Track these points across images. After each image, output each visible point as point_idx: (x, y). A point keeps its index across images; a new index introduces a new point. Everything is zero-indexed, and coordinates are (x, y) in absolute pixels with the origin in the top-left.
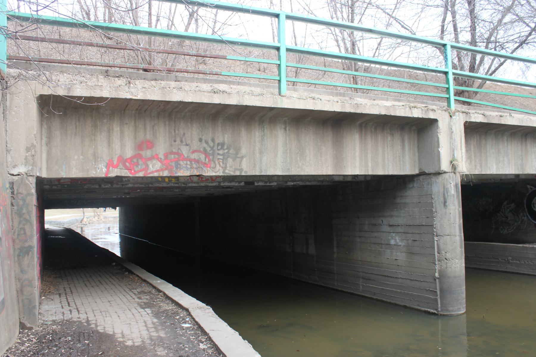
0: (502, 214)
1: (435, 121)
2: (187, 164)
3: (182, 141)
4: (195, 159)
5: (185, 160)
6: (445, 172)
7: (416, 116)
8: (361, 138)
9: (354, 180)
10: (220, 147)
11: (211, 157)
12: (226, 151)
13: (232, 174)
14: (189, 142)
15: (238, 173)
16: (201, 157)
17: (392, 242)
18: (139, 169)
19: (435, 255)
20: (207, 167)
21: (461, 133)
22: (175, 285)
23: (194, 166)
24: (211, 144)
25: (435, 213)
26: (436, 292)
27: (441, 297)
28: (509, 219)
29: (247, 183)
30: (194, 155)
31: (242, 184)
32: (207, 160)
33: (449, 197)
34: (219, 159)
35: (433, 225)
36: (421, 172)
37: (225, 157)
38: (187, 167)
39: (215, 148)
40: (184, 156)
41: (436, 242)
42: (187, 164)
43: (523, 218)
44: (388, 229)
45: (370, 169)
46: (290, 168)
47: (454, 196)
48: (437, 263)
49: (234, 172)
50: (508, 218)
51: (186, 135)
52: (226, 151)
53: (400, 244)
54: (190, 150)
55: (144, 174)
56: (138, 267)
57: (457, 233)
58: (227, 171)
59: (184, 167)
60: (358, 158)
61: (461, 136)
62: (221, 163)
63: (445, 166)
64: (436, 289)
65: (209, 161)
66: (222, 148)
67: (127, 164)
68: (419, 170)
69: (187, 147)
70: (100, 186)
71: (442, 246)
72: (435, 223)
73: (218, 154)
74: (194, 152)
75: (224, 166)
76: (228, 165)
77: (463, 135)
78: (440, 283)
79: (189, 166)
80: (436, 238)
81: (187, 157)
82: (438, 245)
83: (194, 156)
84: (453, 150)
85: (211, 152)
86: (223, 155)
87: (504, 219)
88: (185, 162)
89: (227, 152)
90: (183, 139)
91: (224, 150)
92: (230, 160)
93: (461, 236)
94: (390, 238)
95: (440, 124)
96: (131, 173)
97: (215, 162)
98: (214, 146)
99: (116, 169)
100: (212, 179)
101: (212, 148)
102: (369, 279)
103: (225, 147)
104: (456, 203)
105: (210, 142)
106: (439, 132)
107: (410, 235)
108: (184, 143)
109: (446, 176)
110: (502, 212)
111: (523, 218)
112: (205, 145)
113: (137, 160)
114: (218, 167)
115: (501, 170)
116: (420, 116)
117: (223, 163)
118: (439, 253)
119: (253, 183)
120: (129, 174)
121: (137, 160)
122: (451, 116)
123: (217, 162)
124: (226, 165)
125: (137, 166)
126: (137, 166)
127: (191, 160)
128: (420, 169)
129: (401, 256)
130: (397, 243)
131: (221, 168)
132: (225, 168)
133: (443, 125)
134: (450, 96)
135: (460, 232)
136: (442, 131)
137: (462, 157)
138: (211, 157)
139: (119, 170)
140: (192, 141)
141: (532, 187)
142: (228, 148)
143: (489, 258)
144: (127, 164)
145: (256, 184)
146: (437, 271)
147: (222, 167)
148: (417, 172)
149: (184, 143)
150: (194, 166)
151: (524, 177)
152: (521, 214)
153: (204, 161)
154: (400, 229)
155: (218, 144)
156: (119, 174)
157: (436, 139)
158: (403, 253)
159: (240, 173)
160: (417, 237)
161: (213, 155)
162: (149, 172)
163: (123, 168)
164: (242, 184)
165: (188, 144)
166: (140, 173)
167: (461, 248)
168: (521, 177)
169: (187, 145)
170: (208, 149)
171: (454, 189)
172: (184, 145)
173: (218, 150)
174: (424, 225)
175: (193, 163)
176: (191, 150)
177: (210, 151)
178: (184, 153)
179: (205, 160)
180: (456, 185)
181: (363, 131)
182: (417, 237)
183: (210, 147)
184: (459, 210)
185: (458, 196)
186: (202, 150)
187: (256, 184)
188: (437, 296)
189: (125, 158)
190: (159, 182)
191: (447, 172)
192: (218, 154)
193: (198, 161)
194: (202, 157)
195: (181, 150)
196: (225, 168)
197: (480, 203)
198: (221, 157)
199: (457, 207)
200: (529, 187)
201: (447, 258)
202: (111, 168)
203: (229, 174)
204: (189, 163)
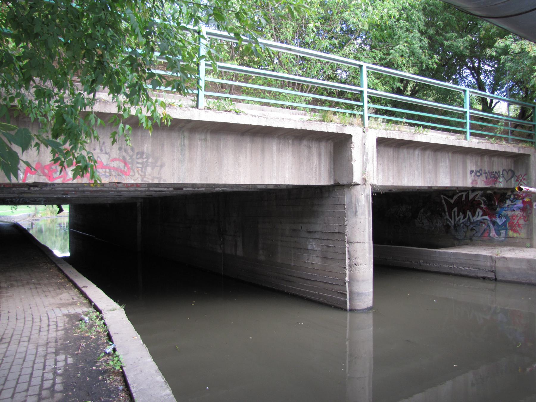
0: (419, 221)
1: (350, 136)
2: (105, 172)
3: (101, 150)
4: (114, 167)
5: (105, 168)
6: (357, 184)
7: (331, 131)
8: (278, 149)
9: (276, 188)
10: (139, 156)
11: (130, 165)
12: (145, 160)
13: (150, 181)
14: (108, 150)
15: (156, 181)
16: (120, 165)
17: (310, 247)
18: (57, 176)
19: (345, 260)
20: (126, 175)
21: (373, 148)
22: (98, 286)
23: (113, 173)
24: (131, 153)
25: (347, 222)
26: (346, 294)
27: (350, 299)
28: (425, 225)
29: (175, 189)
30: (113, 163)
31: (171, 189)
32: (126, 168)
33: (360, 208)
34: (138, 167)
35: (345, 233)
36: (336, 183)
37: (144, 165)
38: (105, 174)
39: (135, 157)
40: (103, 164)
41: (347, 248)
42: (105, 172)
43: (436, 224)
44: (307, 235)
45: (286, 179)
46: (208, 177)
47: (364, 207)
48: (347, 267)
49: (153, 180)
50: (423, 224)
51: (106, 144)
52: (145, 160)
53: (316, 249)
54: (109, 158)
55: (63, 181)
56: (71, 266)
57: (367, 240)
58: (145, 179)
59: (103, 175)
60: (275, 169)
61: (373, 150)
62: (140, 172)
63: (357, 178)
64: (346, 292)
65: (128, 169)
66: (142, 157)
67: (46, 171)
68: (334, 181)
69: (107, 155)
70: (29, 189)
71: (352, 253)
72: (346, 231)
73: (138, 163)
74: (114, 160)
75: (143, 174)
76: (147, 173)
77: (375, 149)
78: (350, 286)
79: (108, 174)
80: (347, 245)
81: (107, 165)
82: (348, 251)
83: (115, 164)
84: (365, 165)
85: (130, 161)
86: (142, 163)
87: (420, 225)
88: (104, 170)
89: (146, 161)
90: (103, 148)
91: (143, 159)
92: (149, 169)
93: (369, 243)
94: (308, 243)
95: (354, 139)
96: (49, 180)
97: (134, 170)
98: (133, 155)
99: (34, 176)
100: (127, 185)
101: (131, 157)
102: (290, 281)
103: (145, 156)
104: (367, 213)
105: (129, 151)
106: (352, 146)
107: (325, 241)
108: (104, 152)
109: (358, 187)
110: (419, 219)
111: (436, 224)
112: (124, 154)
113: (56, 167)
114: (137, 175)
115: (411, 182)
116: (335, 131)
117: (142, 172)
118: (349, 259)
119: (182, 189)
120: (47, 180)
121: (56, 167)
122: (364, 132)
123: (136, 171)
124: (145, 173)
125: (56, 173)
126: (56, 173)
127: (110, 168)
128: (335, 180)
129: (317, 261)
130: (314, 248)
131: (139, 176)
132: (143, 177)
133: (356, 141)
134: (364, 113)
135: (369, 240)
136: (355, 145)
137: (374, 170)
138: (130, 165)
139: (37, 176)
140: (111, 150)
141: (445, 197)
142: (147, 157)
143: (404, 261)
144: (46, 171)
145: (184, 189)
146: (347, 275)
147: (141, 175)
148: (332, 183)
149: (104, 152)
150: (113, 173)
151: (436, 188)
152: (435, 221)
153: (123, 169)
154: (317, 236)
155: (138, 153)
156: (37, 181)
157: (350, 153)
158: (318, 258)
159: (159, 181)
160: (330, 243)
161: (132, 164)
162: (68, 178)
163: (42, 175)
164: (171, 189)
165: (107, 152)
166: (59, 179)
167: (370, 254)
168: (433, 188)
169: (106, 153)
170: (128, 158)
171: (365, 200)
172: (104, 153)
173: (138, 159)
174: (336, 233)
175: (112, 171)
176: (111, 159)
177: (129, 159)
178: (103, 161)
179: (125, 168)
180: (367, 197)
181: (187, 153)
182: (330, 243)
183: (130, 156)
184: (369, 219)
185: (369, 206)
186: (121, 158)
187: (184, 189)
188: (346, 298)
189: (43, 165)
190: (85, 186)
191: (359, 184)
192: (138, 163)
193: (115, 169)
194: (122, 165)
195: (100, 158)
196: (143, 177)
197: (401, 209)
198: (140, 166)
199: (367, 217)
200: (442, 196)
201: (356, 263)
202: (29, 174)
203: (147, 181)
204: (108, 170)
